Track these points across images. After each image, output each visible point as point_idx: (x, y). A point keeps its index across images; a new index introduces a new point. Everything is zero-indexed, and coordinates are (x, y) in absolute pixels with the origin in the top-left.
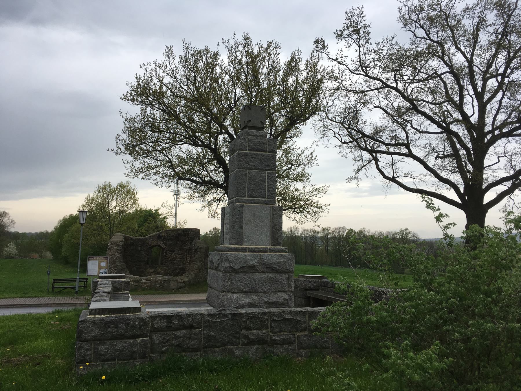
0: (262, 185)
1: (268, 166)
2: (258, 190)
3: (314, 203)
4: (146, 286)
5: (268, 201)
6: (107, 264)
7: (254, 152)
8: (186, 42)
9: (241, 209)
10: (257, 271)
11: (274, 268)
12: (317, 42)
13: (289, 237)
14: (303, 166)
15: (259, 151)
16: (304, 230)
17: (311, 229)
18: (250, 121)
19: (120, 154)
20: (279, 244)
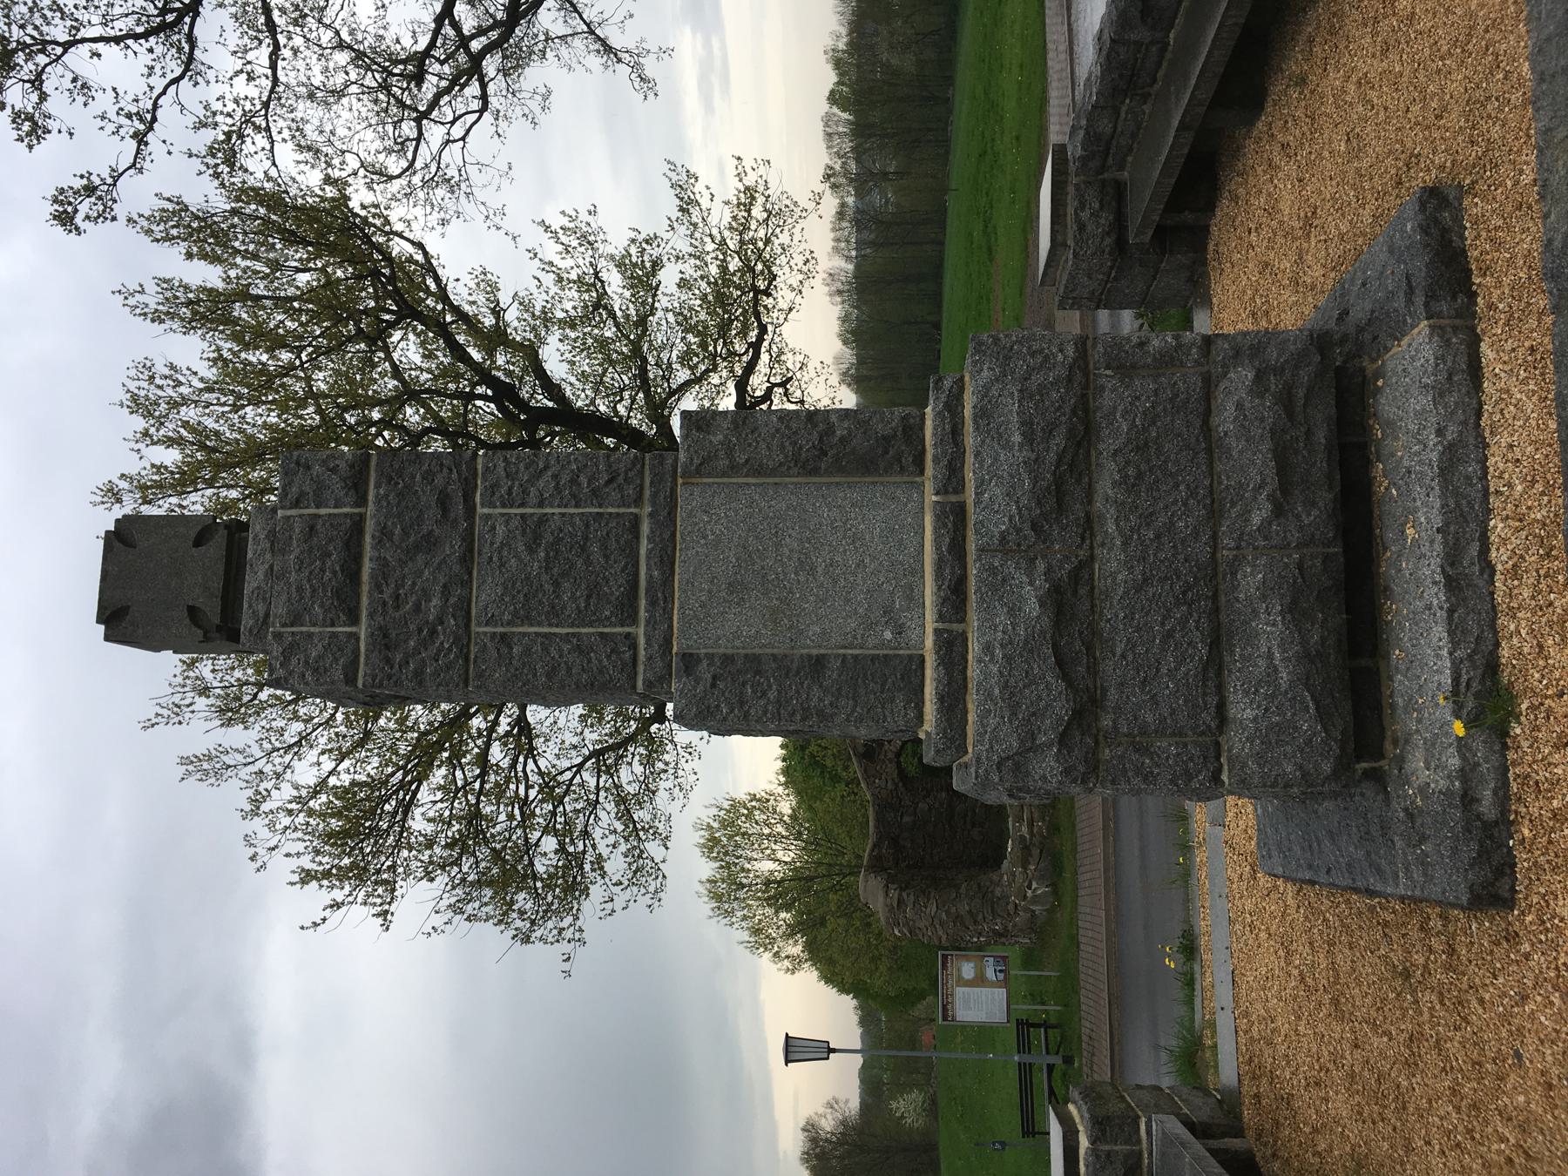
0: (558, 540)
1: (444, 502)
2: (588, 562)
3: (735, 218)
4: (1043, 820)
5: (655, 495)
6: (968, 959)
7: (365, 588)
8: (152, 716)
9: (705, 671)
10: (1082, 572)
11: (1060, 457)
12: (65, 219)
13: (858, 300)
14: (602, 263)
15: (357, 559)
16: (836, 250)
17: (834, 230)
18: (193, 612)
19: (581, 930)
20: (912, 431)
